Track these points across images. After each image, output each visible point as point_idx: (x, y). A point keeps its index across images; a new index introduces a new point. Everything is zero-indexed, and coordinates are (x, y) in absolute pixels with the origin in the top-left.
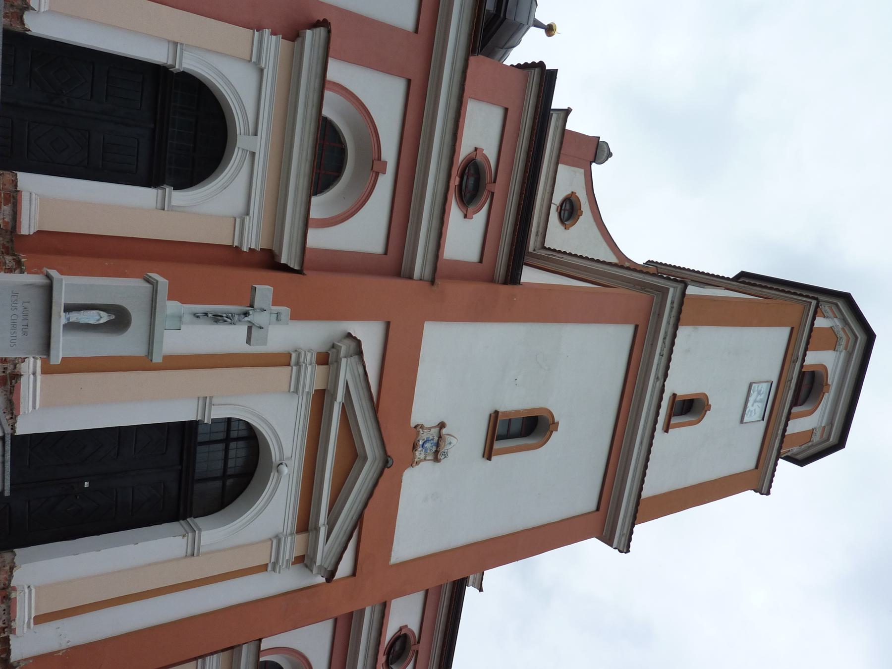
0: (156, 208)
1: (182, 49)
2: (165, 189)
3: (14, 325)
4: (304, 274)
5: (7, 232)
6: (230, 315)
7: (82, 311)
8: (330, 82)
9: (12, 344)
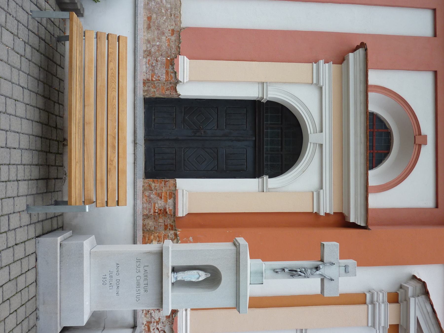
0: (259, 191)
1: (267, 86)
2: (264, 177)
3: (138, 285)
4: (369, 229)
5: (172, 216)
6: (303, 269)
7: (186, 272)
8: (372, 86)
9: (138, 299)
